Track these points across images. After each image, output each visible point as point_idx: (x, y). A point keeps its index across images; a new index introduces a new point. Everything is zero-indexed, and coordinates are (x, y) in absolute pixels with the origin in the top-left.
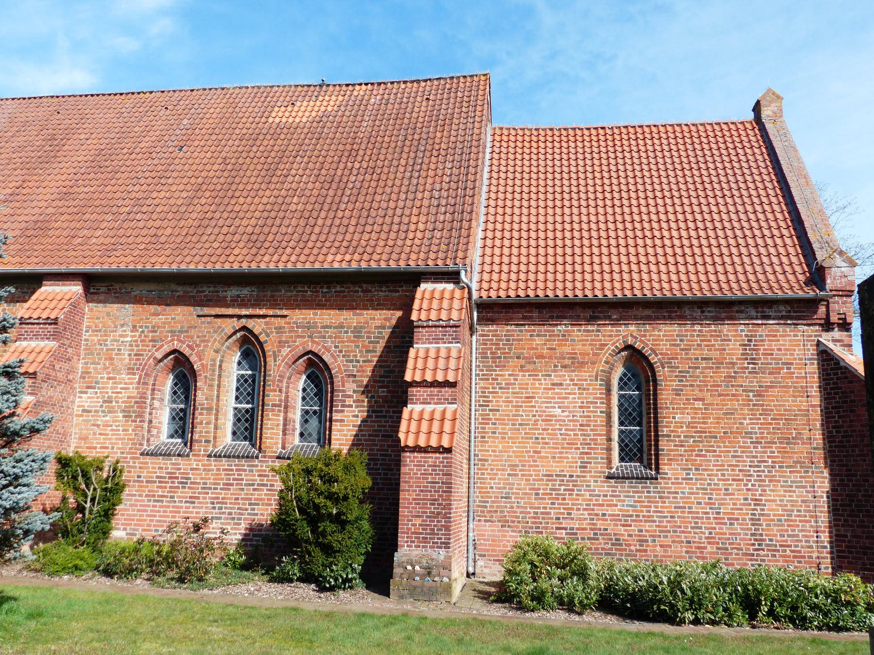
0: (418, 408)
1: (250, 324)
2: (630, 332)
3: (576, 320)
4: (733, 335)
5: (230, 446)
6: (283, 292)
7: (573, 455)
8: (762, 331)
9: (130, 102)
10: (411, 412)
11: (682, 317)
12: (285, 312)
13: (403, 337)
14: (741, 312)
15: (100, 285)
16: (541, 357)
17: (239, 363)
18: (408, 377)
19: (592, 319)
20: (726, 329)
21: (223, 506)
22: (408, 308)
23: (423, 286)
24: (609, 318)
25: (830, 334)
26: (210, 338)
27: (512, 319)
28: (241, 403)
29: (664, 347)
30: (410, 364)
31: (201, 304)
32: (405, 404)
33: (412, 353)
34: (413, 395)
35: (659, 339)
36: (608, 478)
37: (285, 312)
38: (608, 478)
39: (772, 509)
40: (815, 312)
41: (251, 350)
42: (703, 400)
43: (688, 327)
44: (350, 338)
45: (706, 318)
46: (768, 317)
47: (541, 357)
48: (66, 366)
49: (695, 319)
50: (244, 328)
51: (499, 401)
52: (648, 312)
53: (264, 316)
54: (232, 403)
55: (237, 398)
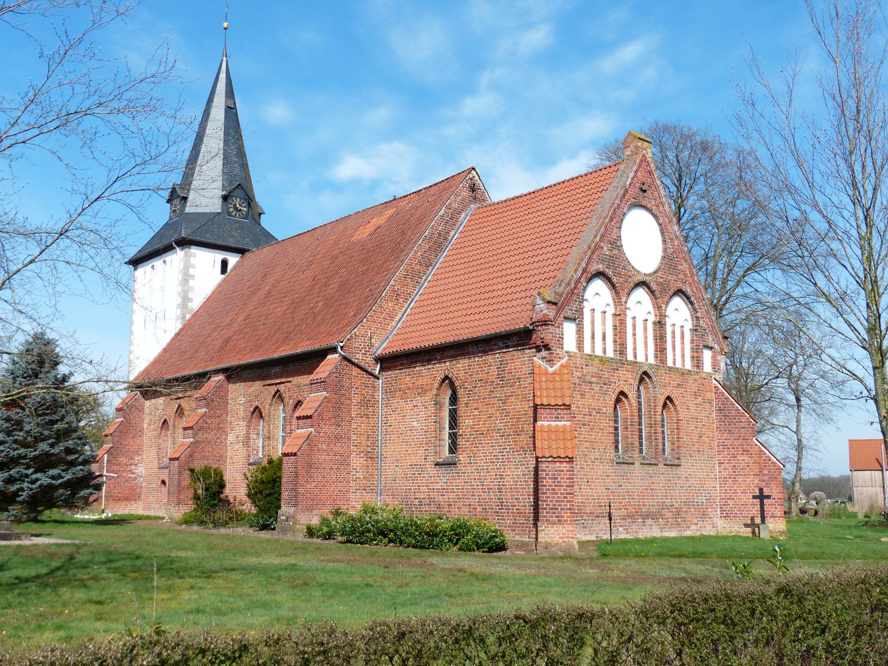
2: (439, 369)
3: (403, 366)
4: (493, 359)
6: (245, 374)
7: (421, 452)
8: (508, 357)
9: (306, 237)
11: (468, 354)
14: (495, 345)
15: (234, 374)
16: (409, 389)
19: (429, 361)
20: (489, 358)
24: (435, 359)
25: (539, 355)
27: (396, 366)
29: (462, 374)
31: (264, 379)
35: (459, 368)
36: (436, 465)
37: (289, 379)
38: (436, 465)
39: (508, 481)
40: (531, 339)
42: (478, 409)
43: (473, 359)
45: (480, 352)
46: (507, 347)
47: (409, 389)
48: (217, 420)
49: (474, 354)
51: (392, 420)
52: (453, 352)
53: (283, 383)
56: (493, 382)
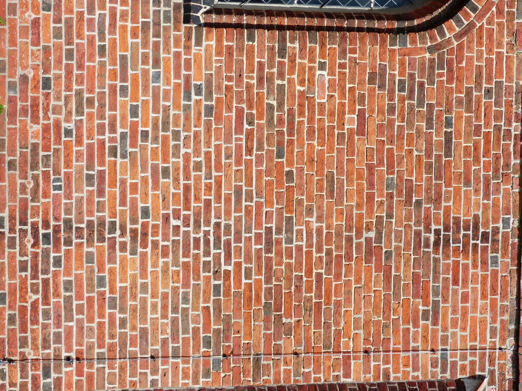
42: (361, 130)
56: (437, 201)
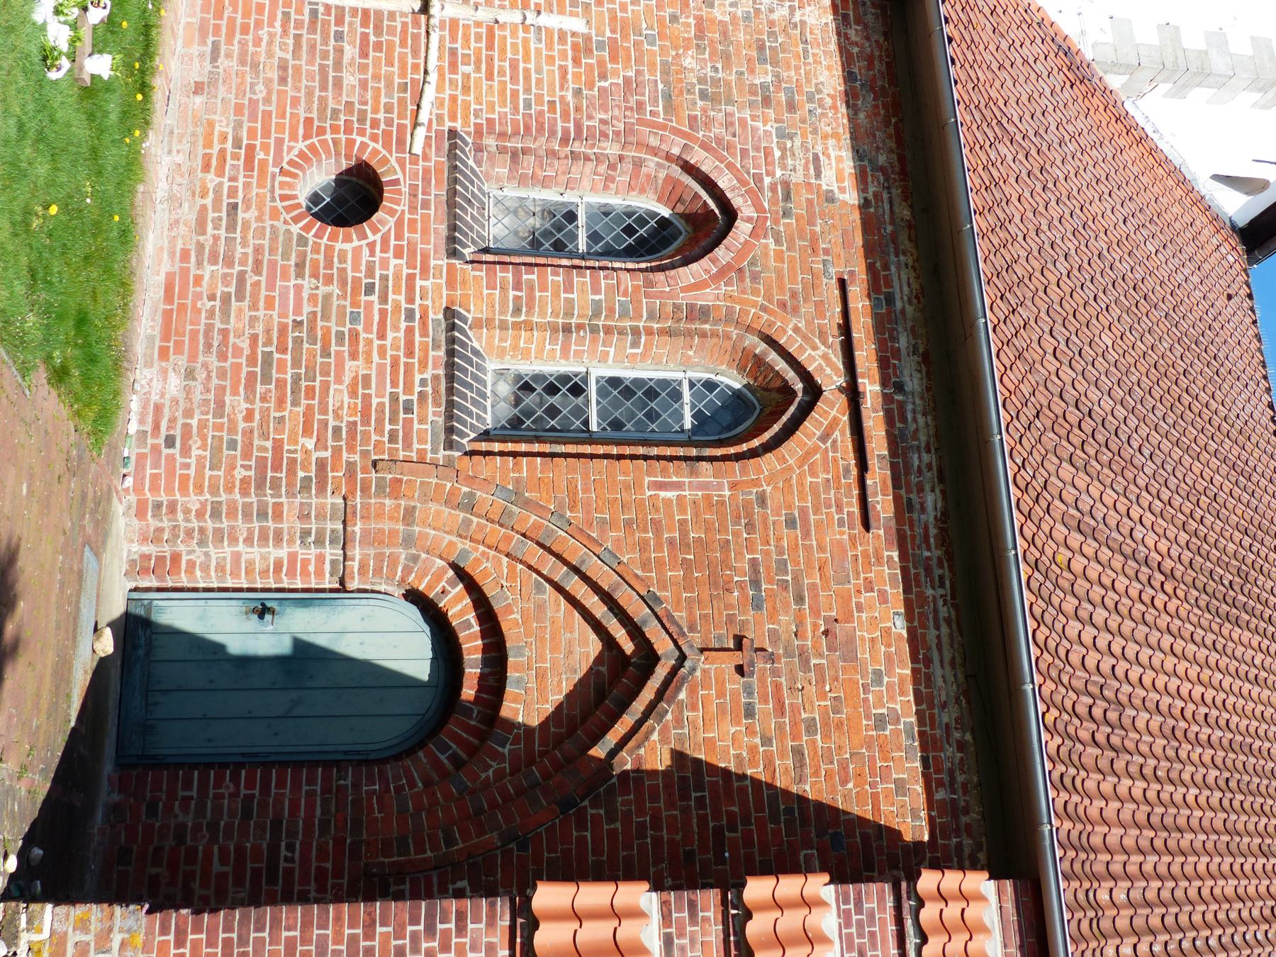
0: (828, 921)
1: (832, 408)
5: (479, 367)
10: (807, 903)
12: (883, 505)
13: (855, 851)
17: (710, 385)
18: (547, 896)
21: (534, 76)
22: (939, 855)
23: (980, 882)
26: (804, 264)
28: (602, 392)
30: (594, 894)
32: (839, 877)
33: (819, 886)
34: (307, 925)
41: (759, 412)
44: (834, 705)
50: (814, 391)
54: (599, 371)
55: (614, 382)
